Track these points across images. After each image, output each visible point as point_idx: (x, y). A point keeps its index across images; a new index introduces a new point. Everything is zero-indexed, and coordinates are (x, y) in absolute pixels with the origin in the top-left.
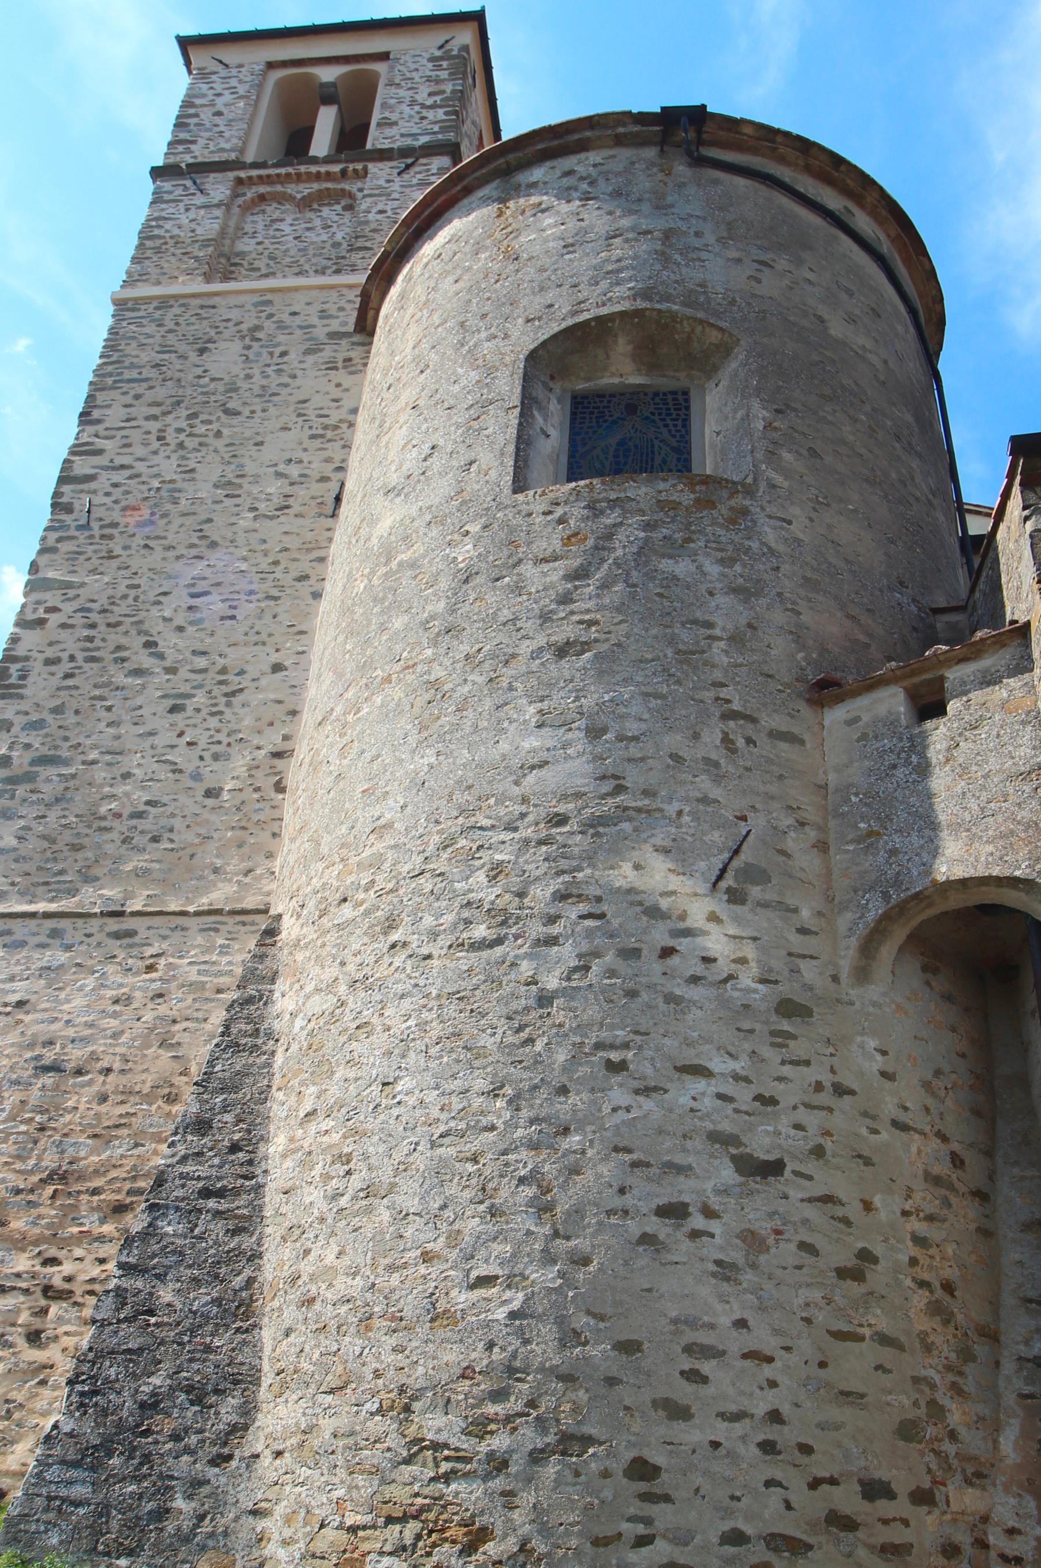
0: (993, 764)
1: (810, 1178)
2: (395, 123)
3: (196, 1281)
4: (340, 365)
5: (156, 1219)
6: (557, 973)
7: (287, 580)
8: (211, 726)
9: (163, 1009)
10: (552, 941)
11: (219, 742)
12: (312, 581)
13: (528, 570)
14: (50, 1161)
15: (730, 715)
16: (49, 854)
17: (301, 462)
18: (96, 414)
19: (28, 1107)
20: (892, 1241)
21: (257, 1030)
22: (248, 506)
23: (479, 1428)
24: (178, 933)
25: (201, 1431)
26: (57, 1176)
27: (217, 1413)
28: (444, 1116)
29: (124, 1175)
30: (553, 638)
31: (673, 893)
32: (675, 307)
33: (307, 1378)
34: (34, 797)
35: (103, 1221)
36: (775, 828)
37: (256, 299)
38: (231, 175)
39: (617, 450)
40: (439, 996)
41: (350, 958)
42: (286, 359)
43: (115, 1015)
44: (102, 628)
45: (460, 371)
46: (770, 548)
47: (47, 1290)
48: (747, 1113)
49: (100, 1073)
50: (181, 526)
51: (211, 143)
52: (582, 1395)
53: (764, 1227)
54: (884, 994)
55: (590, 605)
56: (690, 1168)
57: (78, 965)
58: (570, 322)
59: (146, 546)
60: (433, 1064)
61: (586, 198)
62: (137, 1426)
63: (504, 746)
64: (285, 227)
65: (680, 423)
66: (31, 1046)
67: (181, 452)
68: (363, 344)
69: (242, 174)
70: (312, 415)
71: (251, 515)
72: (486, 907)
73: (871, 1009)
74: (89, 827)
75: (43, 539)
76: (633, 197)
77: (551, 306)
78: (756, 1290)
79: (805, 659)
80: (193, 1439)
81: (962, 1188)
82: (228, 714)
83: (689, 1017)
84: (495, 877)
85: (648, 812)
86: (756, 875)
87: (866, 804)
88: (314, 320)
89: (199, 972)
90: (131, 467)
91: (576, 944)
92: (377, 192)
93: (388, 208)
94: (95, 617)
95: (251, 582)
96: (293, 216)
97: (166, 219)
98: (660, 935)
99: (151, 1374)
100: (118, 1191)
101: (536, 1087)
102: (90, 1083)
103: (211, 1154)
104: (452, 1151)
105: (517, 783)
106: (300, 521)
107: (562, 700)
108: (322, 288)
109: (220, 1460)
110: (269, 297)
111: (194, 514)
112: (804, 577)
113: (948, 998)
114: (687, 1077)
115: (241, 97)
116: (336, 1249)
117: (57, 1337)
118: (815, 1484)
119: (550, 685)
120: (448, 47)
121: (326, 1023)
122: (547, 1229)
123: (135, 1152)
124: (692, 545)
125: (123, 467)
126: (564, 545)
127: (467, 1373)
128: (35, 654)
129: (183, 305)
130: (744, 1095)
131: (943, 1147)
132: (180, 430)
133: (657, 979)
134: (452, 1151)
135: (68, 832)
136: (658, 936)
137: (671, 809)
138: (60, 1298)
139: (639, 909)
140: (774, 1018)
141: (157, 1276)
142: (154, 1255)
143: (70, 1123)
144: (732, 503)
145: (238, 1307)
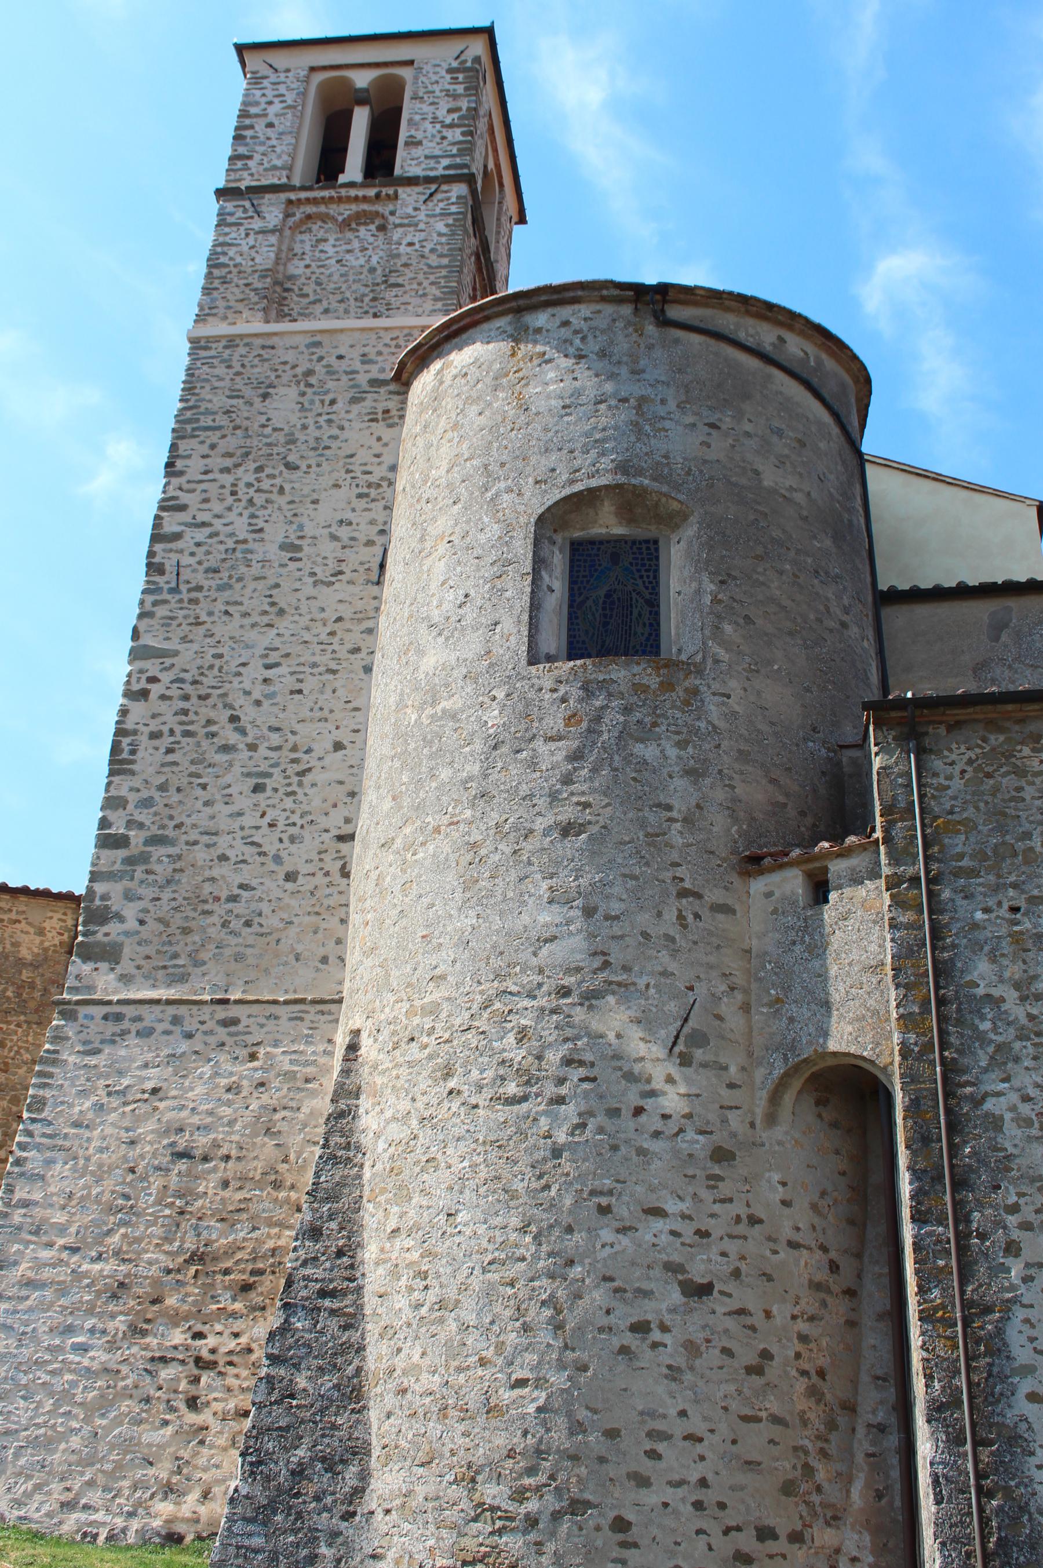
0: (854, 956)
1: (730, 1295)
2: (420, 143)
3: (320, 1369)
4: (380, 416)
5: (289, 1316)
6: (565, 1129)
7: (343, 653)
8: (287, 807)
9: (265, 1098)
10: (560, 1100)
11: (294, 824)
12: (363, 654)
13: (539, 744)
14: (190, 1245)
15: (683, 893)
16: (164, 938)
17: (350, 524)
18: (179, 464)
19: (170, 1192)
20: (784, 1341)
21: (349, 1143)
22: (307, 570)
23: (519, 1495)
24: (273, 1022)
25: (333, 1493)
26: (196, 1258)
27: (343, 1479)
28: (491, 1247)
29: (247, 1257)
30: (559, 818)
31: (642, 1059)
32: (646, 482)
33: (405, 1453)
34: (151, 877)
35: (234, 1299)
36: (713, 995)
37: (309, 340)
38: (283, 196)
39: (604, 603)
40: (484, 1142)
41: (419, 1097)
42: (335, 408)
43: (229, 1103)
44: (194, 700)
45: (486, 520)
46: (714, 727)
47: (198, 1360)
48: (691, 1246)
49: (222, 1159)
50: (255, 590)
51: (266, 159)
52: (583, 1470)
53: (699, 1337)
54: (786, 1133)
55: (585, 787)
56: (652, 1292)
57: (196, 1052)
58: (568, 491)
59: (227, 613)
60: (482, 1201)
61: (580, 357)
62: (291, 1489)
63: (526, 919)
64: (328, 247)
65: (651, 574)
66: (167, 1132)
67: (251, 510)
68: (398, 393)
69: (293, 196)
70: (358, 470)
71: (311, 580)
72: (516, 1067)
73: (777, 1148)
74: (195, 910)
75: (142, 603)
76: (615, 359)
77: (553, 470)
78: (693, 1387)
79: (738, 831)
80: (329, 1499)
81: (836, 1289)
82: (300, 797)
83: (653, 1167)
84: (521, 1040)
85: (626, 986)
86: (699, 1039)
87: (776, 974)
88: (357, 365)
89: (291, 1062)
90: (210, 525)
91: (577, 1104)
92: (406, 221)
93: (416, 240)
94: (188, 688)
95: (314, 654)
96: (335, 236)
97: (230, 245)
98: (633, 1099)
99: (296, 1448)
100: (243, 1271)
101: (551, 1226)
102: (215, 1169)
103: (323, 1258)
104: (496, 1277)
105: (535, 954)
106: (351, 588)
107: (566, 880)
108: (363, 330)
109: (349, 1516)
110: (318, 338)
111: (265, 578)
112: (740, 751)
113: (834, 1125)
114: (651, 1218)
115: (289, 107)
116: (420, 1351)
117: (208, 1402)
118: (727, 1531)
119: (558, 864)
120: (462, 58)
121: (404, 1151)
122: (558, 1343)
123: (253, 1235)
124: (657, 729)
125: (204, 524)
126: (566, 725)
127: (511, 1454)
128: (140, 727)
129: (247, 345)
130: (688, 1230)
131: (824, 1257)
132: (249, 485)
133: (632, 1135)
134: (496, 1277)
135: (178, 915)
136: (632, 1097)
137: (642, 982)
138: (207, 1368)
139: (619, 1073)
140: (709, 1164)
141: (294, 1365)
142: (289, 1349)
143: (202, 1207)
144: (687, 684)
145: (352, 1392)
